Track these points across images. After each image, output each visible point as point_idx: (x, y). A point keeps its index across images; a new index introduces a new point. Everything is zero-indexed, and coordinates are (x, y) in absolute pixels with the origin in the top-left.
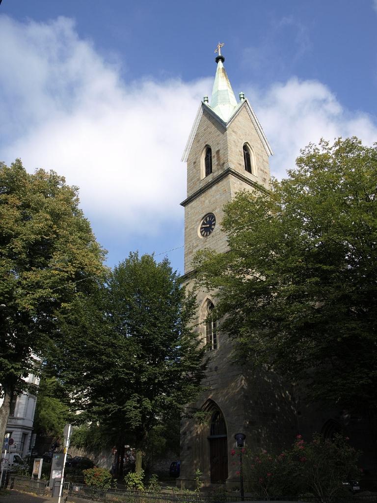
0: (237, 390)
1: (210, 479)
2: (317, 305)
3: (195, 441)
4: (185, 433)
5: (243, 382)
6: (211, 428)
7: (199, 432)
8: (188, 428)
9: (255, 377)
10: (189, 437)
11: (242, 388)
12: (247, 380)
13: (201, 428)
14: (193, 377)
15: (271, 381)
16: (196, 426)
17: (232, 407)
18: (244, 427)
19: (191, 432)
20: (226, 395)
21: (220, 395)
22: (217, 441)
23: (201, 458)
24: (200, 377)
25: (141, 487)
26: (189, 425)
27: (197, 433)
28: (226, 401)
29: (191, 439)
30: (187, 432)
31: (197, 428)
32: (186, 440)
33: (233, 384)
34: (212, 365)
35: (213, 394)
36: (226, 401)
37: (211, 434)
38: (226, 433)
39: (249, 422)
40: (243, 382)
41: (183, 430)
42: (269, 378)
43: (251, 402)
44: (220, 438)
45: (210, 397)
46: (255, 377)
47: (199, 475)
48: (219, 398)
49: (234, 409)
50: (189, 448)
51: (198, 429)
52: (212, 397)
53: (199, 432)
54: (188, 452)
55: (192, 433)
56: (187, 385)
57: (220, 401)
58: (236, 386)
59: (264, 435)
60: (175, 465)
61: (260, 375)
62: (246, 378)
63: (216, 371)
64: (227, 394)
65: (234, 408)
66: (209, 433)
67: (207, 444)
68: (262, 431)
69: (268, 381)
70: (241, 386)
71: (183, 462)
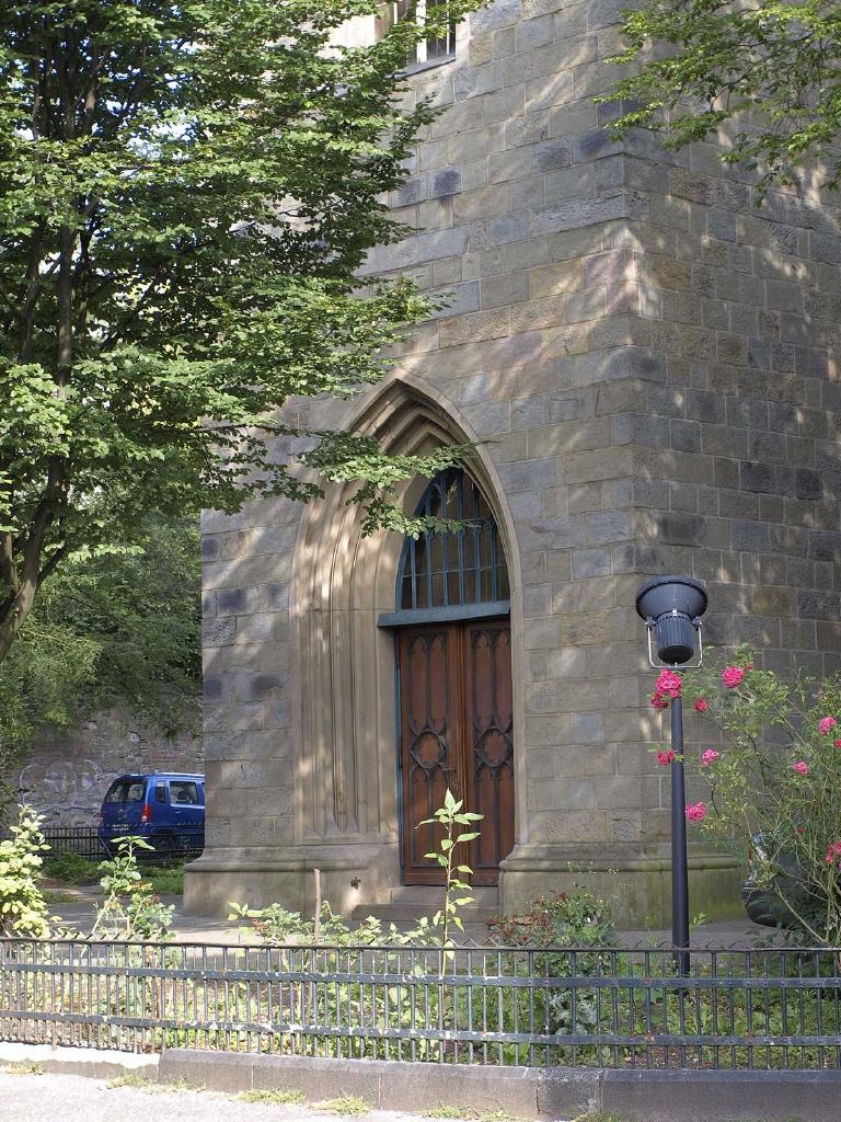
0: (587, 328)
1: (396, 862)
2: (98, 270)
3: (304, 642)
4: (233, 599)
5: (631, 272)
6: (405, 568)
7: (325, 593)
8: (259, 566)
9: (705, 240)
10: (265, 622)
11: (625, 310)
12: (655, 262)
13: (343, 562)
14: (311, 235)
15: (801, 272)
16: (306, 552)
17: (554, 434)
18: (629, 554)
19: (274, 591)
20: (515, 357)
21: (471, 357)
22: (448, 641)
23: (340, 742)
24: (356, 234)
25: (30, 917)
26: (262, 544)
27: (314, 593)
28: (514, 393)
29: (280, 631)
30: (252, 594)
31: (313, 567)
32: (242, 639)
33: (562, 285)
34: (423, 163)
35: (422, 349)
36: (514, 393)
37: (405, 602)
38: (504, 593)
39: (664, 525)
40: (631, 272)
41: (223, 577)
42: (789, 252)
43: (679, 400)
44: (461, 624)
45: (400, 374)
46: (705, 240)
47: (459, 829)
48: (467, 377)
49: (571, 444)
50: (263, 687)
51: (323, 575)
52: (416, 373)
53: (325, 593)
54: (261, 712)
55: (281, 599)
56: (283, 284)
57: (472, 394)
58: (584, 292)
59: (749, 606)
60: (133, 794)
61: (740, 230)
62: (652, 253)
63: (444, 200)
64: (524, 344)
65: (565, 436)
66: (390, 601)
67: (378, 655)
68: (734, 576)
69: (788, 270)
70: (618, 298)
71: (228, 771)
